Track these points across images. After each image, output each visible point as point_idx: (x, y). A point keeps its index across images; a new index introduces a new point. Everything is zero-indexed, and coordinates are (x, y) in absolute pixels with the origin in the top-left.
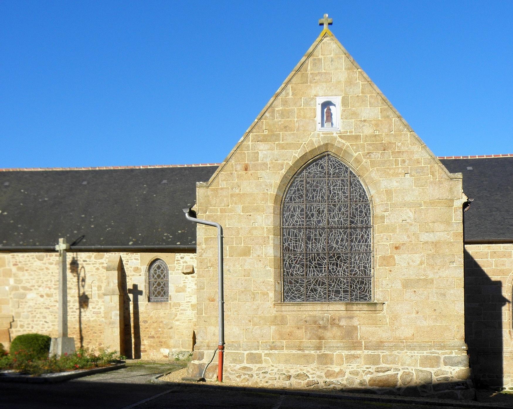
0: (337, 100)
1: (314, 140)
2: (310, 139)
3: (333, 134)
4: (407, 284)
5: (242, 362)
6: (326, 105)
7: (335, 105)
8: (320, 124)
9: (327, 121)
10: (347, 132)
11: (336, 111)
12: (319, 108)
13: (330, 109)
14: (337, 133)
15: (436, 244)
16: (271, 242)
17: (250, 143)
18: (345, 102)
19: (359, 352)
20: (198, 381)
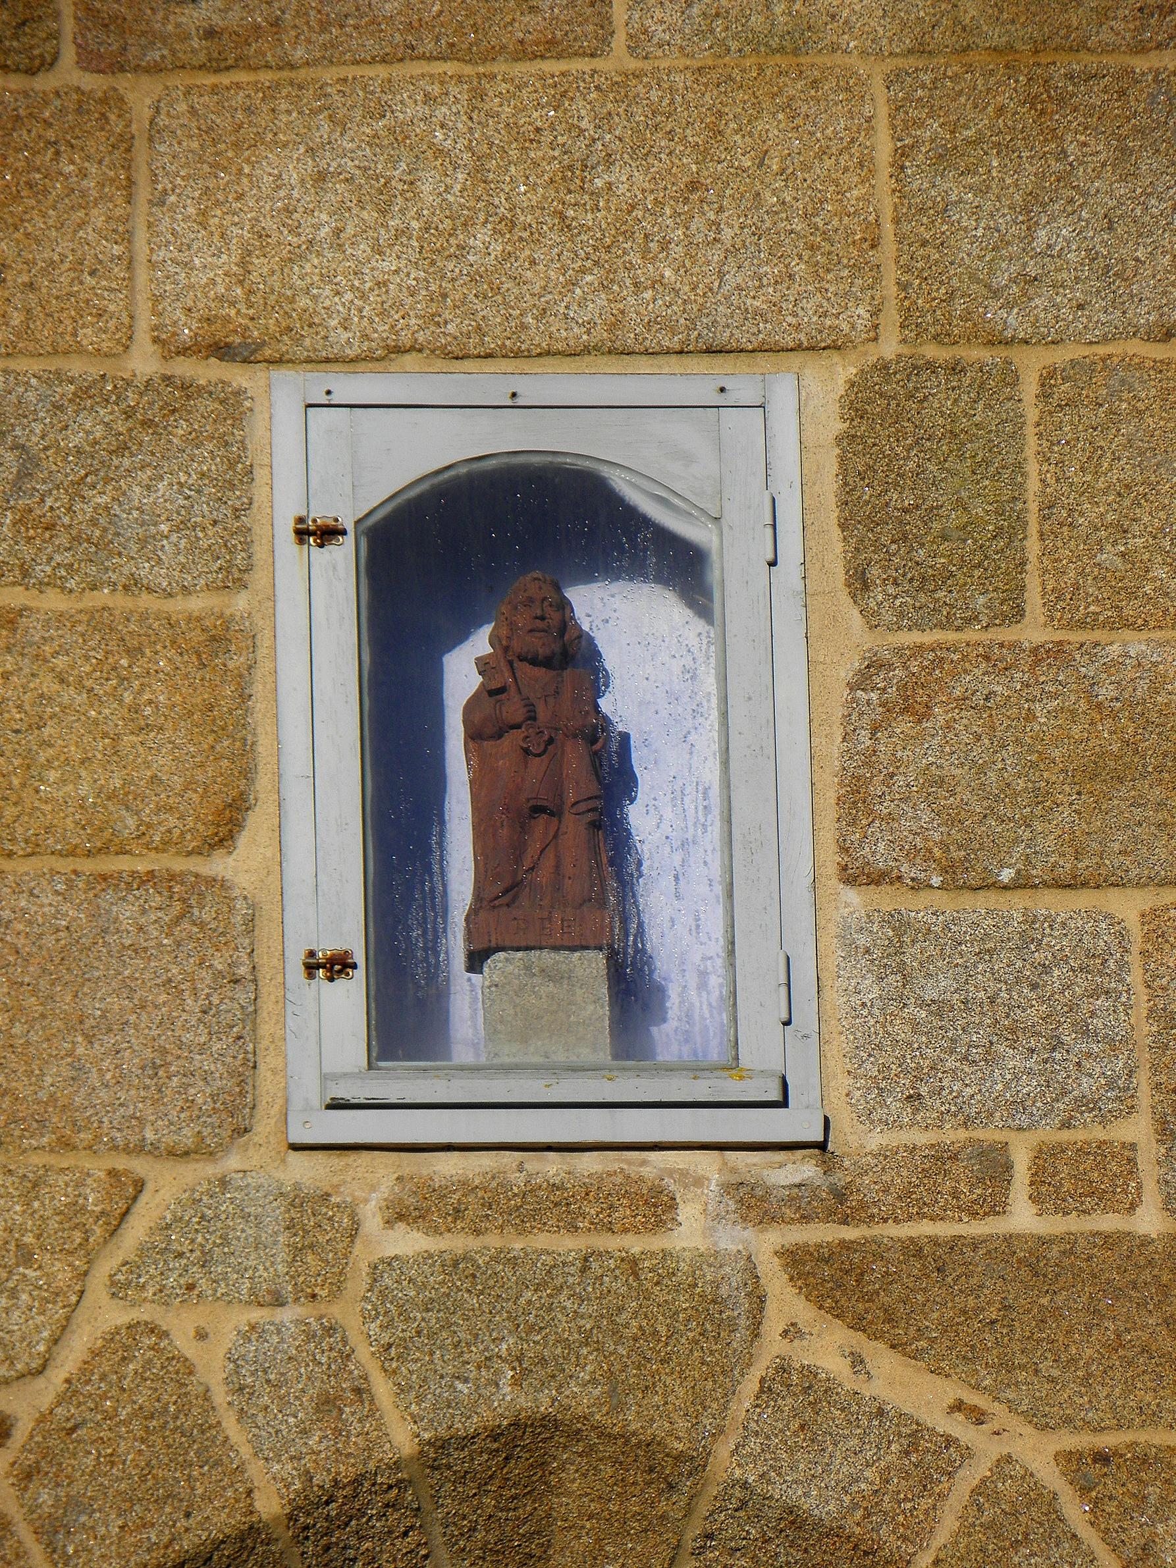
0: (746, 455)
1: (212, 1338)
2: (104, 1315)
3: (658, 1207)
6: (492, 553)
7: (682, 567)
8: (347, 1000)
9: (513, 912)
10: (995, 1167)
11: (719, 710)
13: (571, 658)
14: (753, 1203)
18: (911, 513)
20: (696, 518)
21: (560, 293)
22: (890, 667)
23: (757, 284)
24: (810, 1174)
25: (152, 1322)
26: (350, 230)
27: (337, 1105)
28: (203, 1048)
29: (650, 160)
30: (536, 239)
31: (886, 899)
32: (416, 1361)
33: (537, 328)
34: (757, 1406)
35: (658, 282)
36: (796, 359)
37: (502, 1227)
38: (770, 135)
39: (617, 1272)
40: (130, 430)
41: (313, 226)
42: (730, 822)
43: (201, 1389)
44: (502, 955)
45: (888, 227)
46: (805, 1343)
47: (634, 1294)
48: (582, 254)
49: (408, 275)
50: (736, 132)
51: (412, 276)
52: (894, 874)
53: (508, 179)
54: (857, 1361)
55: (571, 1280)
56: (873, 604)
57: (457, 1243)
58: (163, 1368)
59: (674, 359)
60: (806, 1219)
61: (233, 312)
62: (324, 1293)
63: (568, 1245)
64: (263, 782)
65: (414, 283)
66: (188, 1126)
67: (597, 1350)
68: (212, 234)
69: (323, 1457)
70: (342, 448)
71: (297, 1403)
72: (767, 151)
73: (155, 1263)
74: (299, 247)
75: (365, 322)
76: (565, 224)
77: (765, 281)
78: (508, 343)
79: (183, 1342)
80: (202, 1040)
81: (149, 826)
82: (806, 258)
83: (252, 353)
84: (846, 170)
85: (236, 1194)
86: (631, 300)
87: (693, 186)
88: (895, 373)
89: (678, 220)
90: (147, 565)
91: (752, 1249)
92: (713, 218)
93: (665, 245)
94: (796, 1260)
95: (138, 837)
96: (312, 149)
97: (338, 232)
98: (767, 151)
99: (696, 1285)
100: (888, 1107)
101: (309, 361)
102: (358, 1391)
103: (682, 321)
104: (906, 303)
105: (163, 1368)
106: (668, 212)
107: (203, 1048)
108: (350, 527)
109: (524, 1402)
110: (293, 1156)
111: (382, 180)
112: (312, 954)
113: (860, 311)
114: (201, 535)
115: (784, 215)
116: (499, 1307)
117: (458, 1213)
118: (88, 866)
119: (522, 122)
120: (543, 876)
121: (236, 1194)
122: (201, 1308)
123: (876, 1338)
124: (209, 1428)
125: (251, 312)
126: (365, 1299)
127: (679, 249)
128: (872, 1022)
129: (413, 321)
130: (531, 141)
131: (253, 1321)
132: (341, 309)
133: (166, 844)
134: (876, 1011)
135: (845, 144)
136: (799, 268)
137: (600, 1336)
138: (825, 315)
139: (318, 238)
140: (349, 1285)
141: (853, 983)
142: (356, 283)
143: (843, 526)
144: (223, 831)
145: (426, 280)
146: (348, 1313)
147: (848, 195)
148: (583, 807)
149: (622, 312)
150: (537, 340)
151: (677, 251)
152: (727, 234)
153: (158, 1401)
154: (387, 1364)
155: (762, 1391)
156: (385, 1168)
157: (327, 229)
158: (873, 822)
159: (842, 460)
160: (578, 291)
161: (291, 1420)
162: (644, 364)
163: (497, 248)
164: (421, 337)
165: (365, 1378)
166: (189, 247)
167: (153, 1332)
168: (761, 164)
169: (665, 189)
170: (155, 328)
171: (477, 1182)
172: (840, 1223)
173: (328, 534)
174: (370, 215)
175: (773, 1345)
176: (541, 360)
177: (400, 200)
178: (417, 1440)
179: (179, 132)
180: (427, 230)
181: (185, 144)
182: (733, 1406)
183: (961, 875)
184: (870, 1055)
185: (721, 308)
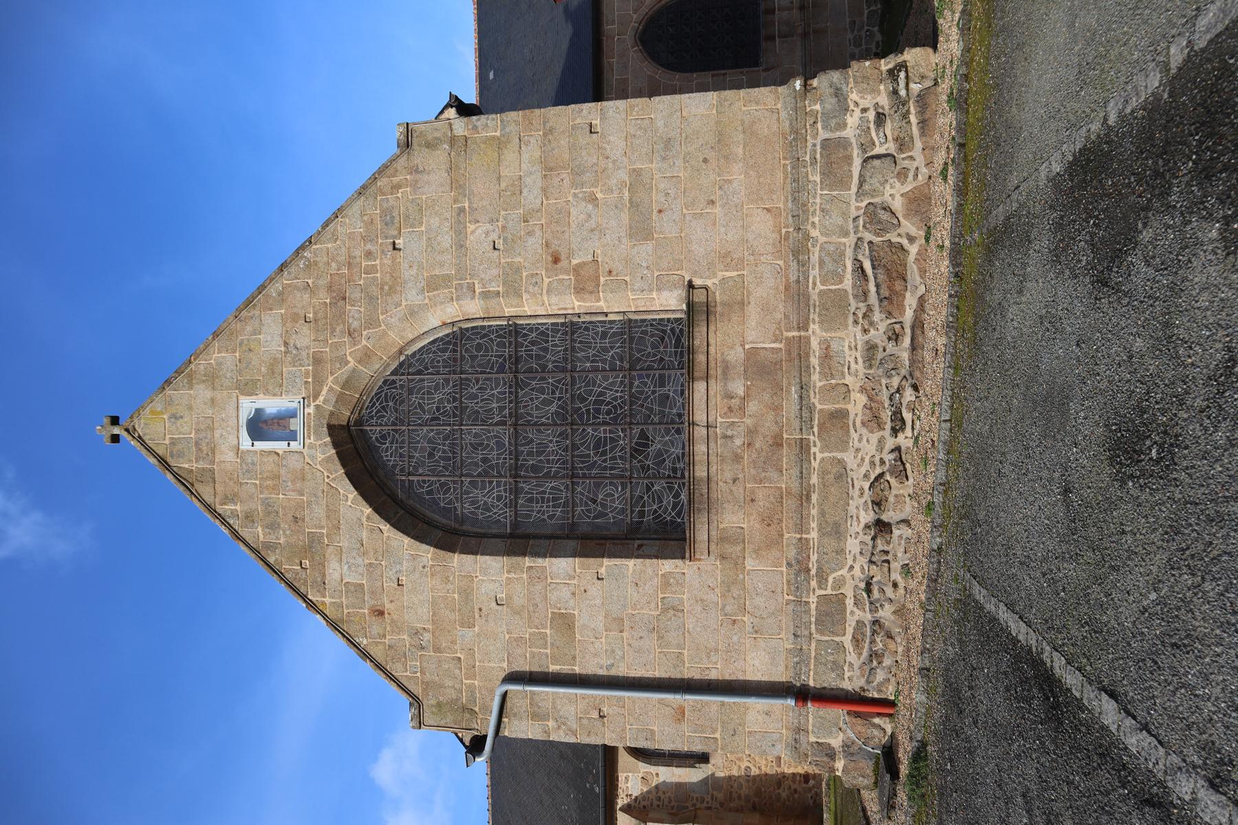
0: (248, 405)
1: (320, 457)
4: (641, 230)
5: (840, 647)
11: (272, 405)
12: (261, 445)
15: (549, 169)
16: (540, 562)
17: (327, 600)
18: (248, 388)
19: (814, 344)
69: (330, 446)
70: (246, 442)
118: (817, 380)
183: (281, 386)
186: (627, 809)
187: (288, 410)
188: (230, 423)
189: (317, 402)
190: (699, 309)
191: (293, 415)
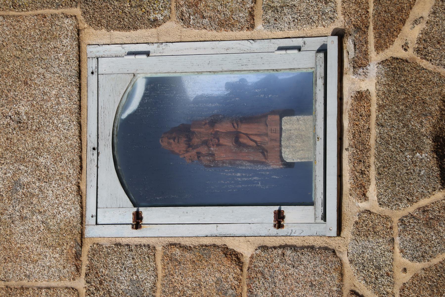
0: (118, 68)
3: (361, 97)
8: (292, 213)
11: (208, 65)
12: (168, 223)
21: (60, 132)
22: (182, 12)
23: (57, 60)
24: (351, 41)
25: (400, 289)
26: (39, 208)
27: (324, 218)
28: (306, 267)
29: (17, 98)
30: (42, 142)
31: (259, 12)
32: (413, 190)
33: (71, 140)
34: (431, 60)
35: (57, 96)
36: (83, 45)
37: (368, 157)
38: (9, 55)
39: (383, 113)
40: (103, 289)
41: (37, 221)
42: (234, 71)
43: (423, 271)
44: (283, 155)
45: (39, 11)
46: (409, 42)
47: (390, 107)
48: (48, 124)
49: (54, 187)
50: (8, 67)
51: (54, 185)
52: (250, 10)
53: (23, 150)
54: (416, 22)
55: (386, 131)
56: (162, 18)
57: (373, 173)
58: (416, 286)
59: (82, 91)
60: (366, 42)
61: (65, 251)
62: (389, 223)
63: (374, 132)
64: (218, 242)
65: (56, 185)
66: (332, 274)
67: (410, 121)
68: (39, 258)
70: (110, 212)
71: (428, 235)
72: (15, 56)
73: (379, 287)
74: (44, 227)
75: (69, 203)
76: (38, 130)
77: (56, 57)
78: (76, 151)
79: (406, 278)
80: (303, 267)
81: (232, 286)
82: (49, 42)
83: (78, 244)
84: (20, 27)
85: (355, 256)
86: (62, 106)
87: (26, 83)
88: (86, 9)
89: (37, 89)
90: (147, 284)
91: (376, 63)
92: (36, 76)
93: (45, 94)
94: (379, 48)
95: (236, 289)
96: (12, 221)
97: (40, 212)
98: (15, 56)
99: (388, 84)
100: (328, 12)
101: (82, 223)
102: (424, 211)
103: (69, 88)
104: (64, 5)
105: (416, 286)
106: (34, 92)
107: (306, 267)
108: (135, 209)
109: (428, 148)
110: (343, 234)
111: (23, 196)
112: (275, 226)
113: (66, 22)
114: (137, 264)
115: (35, 50)
116: (394, 158)
117: (362, 173)
119: (5, 145)
120: (258, 139)
121: (355, 256)
122: (395, 271)
123: (408, 15)
124: (437, 269)
125: (65, 244)
126: (392, 209)
127: (46, 88)
128: (299, 18)
129: (69, 185)
130: (11, 141)
131: (399, 251)
132: (64, 211)
133: (239, 280)
134: (296, 16)
135: (12, 27)
136: (52, 44)
137: (405, 120)
138: (67, 35)
139: (41, 220)
140: (386, 214)
141: (286, 25)
142: (56, 206)
143: (136, 29)
144: (234, 258)
145: (55, 180)
146: (397, 214)
147: (28, 26)
148: (235, 125)
149: (66, 109)
150: (75, 140)
151: (47, 89)
152: (41, 70)
153: (427, 288)
154: (415, 201)
155: (426, 59)
156: (346, 199)
157: (38, 216)
158: (232, 18)
159: (114, 29)
160: (59, 125)
161: (434, 238)
162: (83, 102)
163: (45, 155)
164: (74, 182)
165: (419, 209)
166: (44, 267)
167: (404, 289)
168: (18, 57)
169: (27, 93)
170: (70, 280)
171: (352, 166)
172: (368, 29)
173: (138, 217)
174: (35, 201)
175: (409, 54)
176: (82, 139)
177: (29, 190)
178: (441, 190)
179: (6, 270)
180: (39, 180)
181: (10, 268)
182: (430, 69)
184: (311, 19)
185: (65, 73)
186: (280, 208)
187: (269, 85)
188: (52, 138)
189: (395, 50)
190: (143, 78)
191: (297, 100)
